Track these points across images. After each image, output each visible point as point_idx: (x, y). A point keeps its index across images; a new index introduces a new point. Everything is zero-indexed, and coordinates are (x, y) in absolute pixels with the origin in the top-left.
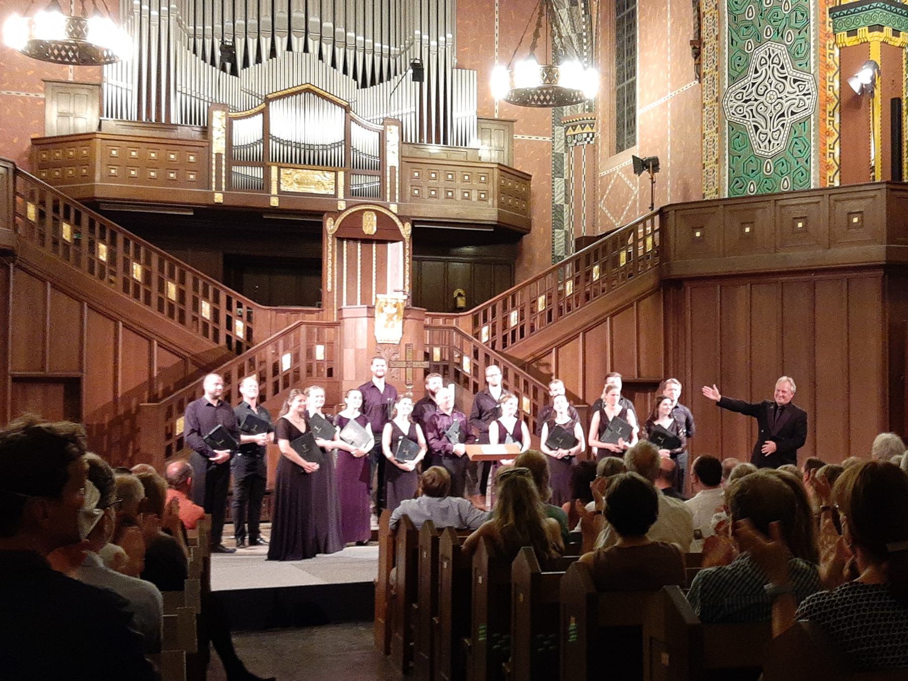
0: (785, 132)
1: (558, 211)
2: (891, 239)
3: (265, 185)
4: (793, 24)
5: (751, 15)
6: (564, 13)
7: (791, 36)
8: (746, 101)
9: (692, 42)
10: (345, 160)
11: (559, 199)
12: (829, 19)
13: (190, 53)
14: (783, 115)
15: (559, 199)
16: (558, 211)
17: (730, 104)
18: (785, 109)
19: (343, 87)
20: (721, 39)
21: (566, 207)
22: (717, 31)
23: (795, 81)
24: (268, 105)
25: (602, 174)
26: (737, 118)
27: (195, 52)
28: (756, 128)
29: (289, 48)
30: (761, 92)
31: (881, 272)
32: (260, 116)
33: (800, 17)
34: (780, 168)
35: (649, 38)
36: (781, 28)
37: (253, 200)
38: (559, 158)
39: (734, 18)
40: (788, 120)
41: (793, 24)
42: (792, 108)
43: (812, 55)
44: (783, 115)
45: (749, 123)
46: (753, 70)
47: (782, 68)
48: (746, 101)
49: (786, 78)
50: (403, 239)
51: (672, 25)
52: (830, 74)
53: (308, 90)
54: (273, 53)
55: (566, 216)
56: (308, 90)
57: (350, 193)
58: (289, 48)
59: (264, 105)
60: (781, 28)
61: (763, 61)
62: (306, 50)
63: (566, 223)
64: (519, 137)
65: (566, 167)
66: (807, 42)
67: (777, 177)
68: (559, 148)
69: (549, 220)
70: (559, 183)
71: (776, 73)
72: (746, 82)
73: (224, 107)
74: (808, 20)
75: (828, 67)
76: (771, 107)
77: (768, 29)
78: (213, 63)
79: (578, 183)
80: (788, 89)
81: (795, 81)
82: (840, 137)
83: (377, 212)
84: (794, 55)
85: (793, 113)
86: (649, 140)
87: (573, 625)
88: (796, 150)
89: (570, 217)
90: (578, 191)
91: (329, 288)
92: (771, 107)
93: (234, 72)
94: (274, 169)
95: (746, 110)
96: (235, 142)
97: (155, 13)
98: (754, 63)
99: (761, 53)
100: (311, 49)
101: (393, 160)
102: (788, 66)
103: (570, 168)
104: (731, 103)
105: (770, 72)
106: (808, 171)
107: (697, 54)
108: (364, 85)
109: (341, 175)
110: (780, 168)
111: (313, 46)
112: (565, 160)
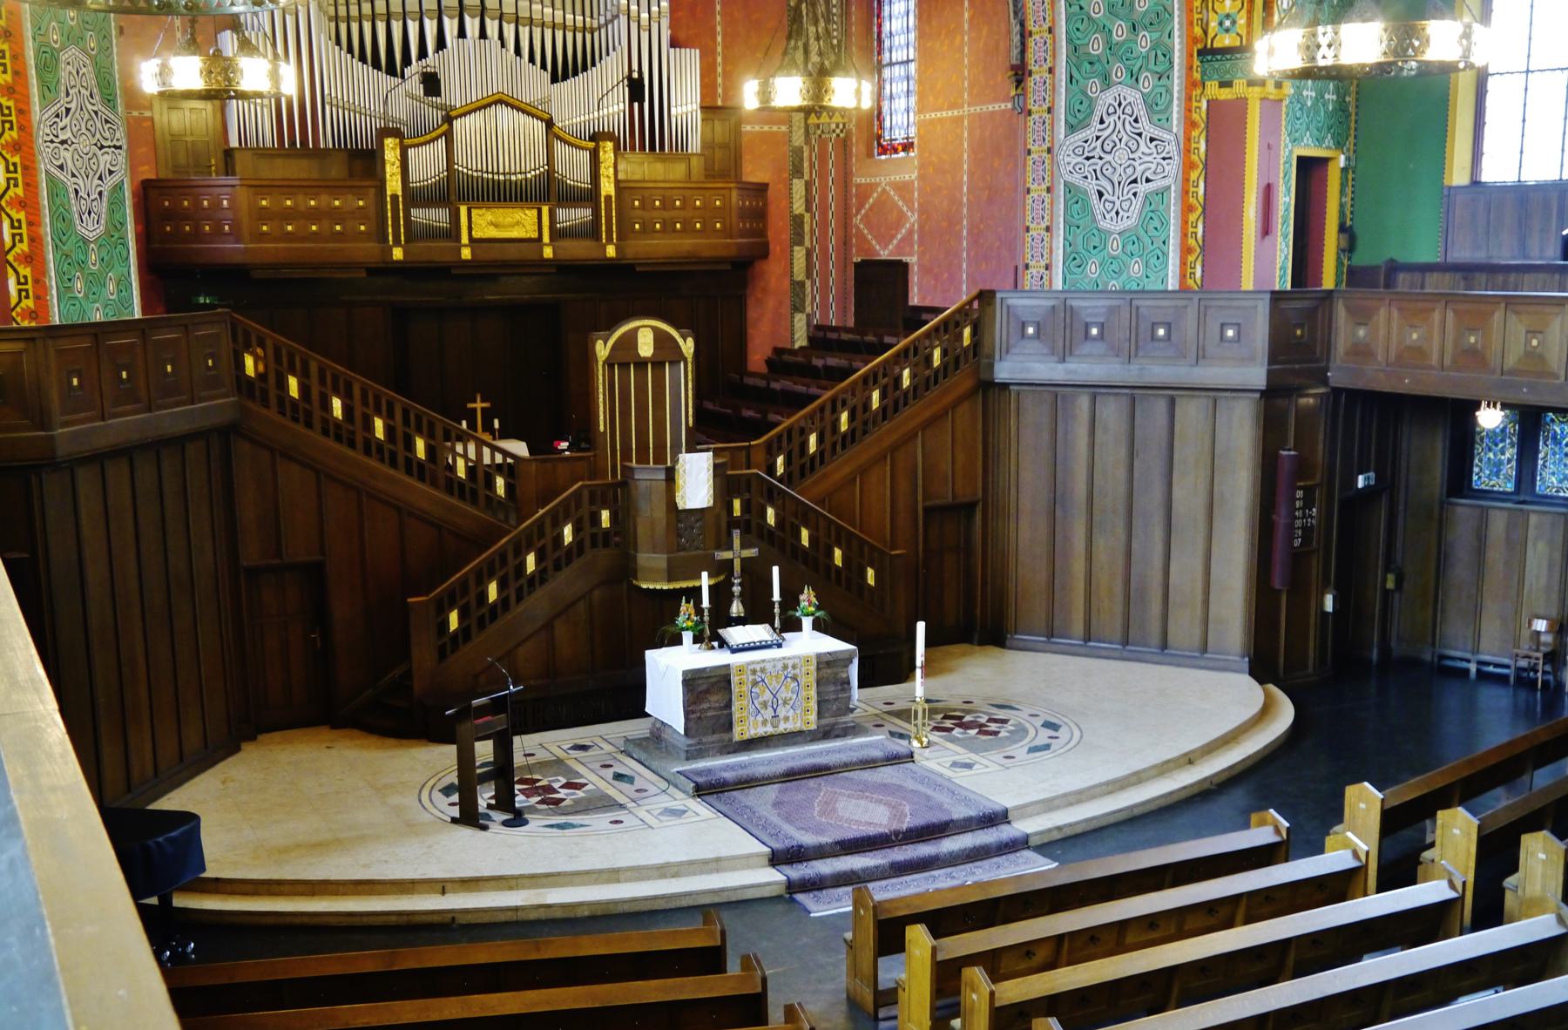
0: (1137, 204)
1: (798, 221)
2: (1273, 359)
3: (453, 233)
4: (1152, 65)
5: (1096, 48)
7: (1148, 83)
8: (1088, 158)
9: (1013, 68)
10: (545, 190)
11: (799, 207)
12: (1196, 62)
13: (331, 44)
14: (1135, 181)
16: (798, 221)
17: (1067, 159)
18: (1138, 174)
19: (534, 84)
20: (1057, 30)
21: (807, 217)
22: (1052, 58)
23: (1152, 140)
24: (451, 125)
25: (857, 180)
26: (1076, 179)
27: (338, 43)
28: (1101, 194)
29: (462, 33)
30: (1108, 148)
31: (1258, 395)
32: (442, 143)
33: (1161, 57)
34: (1130, 247)
35: (934, 23)
36: (1135, 70)
37: (435, 251)
38: (798, 152)
39: (1074, 49)
40: (1142, 188)
41: (1152, 65)
42: (1148, 174)
43: (1175, 109)
44: (1135, 181)
45: (1091, 186)
46: (1097, 119)
47: (1136, 121)
48: (1088, 158)
49: (1140, 135)
50: (685, 360)
51: (971, 19)
52: (1195, 133)
53: (500, 102)
55: (807, 228)
57: (557, 235)
58: (462, 33)
59: (445, 127)
60: (1135, 70)
61: (1111, 110)
62: (483, 35)
63: (807, 238)
64: (748, 128)
65: (806, 164)
66: (1169, 91)
67: (1125, 258)
68: (798, 139)
69: (786, 236)
70: (798, 186)
71: (1128, 127)
72: (1089, 133)
73: (396, 133)
74: (1171, 63)
75: (1193, 125)
76: (1120, 170)
77: (1118, 71)
78: (350, 50)
79: (824, 189)
80: (1143, 148)
81: (1152, 140)
82: (1204, 212)
83: (653, 328)
84: (1151, 106)
85: (1148, 180)
86: (934, 159)
87: (1375, 655)
88: (1151, 227)
89: (812, 232)
90: (824, 198)
91: (602, 428)
92: (1120, 170)
93: (391, 70)
94: (463, 210)
95: (1088, 168)
96: (413, 176)
97: (645, 16)
98: (1100, 110)
99: (1109, 98)
100: (489, 32)
102: (1144, 120)
103: (812, 166)
104: (1068, 158)
105: (1119, 125)
106: (1166, 254)
108: (554, 80)
109: (545, 210)
110: (1130, 247)
111: (492, 27)
112: (806, 154)
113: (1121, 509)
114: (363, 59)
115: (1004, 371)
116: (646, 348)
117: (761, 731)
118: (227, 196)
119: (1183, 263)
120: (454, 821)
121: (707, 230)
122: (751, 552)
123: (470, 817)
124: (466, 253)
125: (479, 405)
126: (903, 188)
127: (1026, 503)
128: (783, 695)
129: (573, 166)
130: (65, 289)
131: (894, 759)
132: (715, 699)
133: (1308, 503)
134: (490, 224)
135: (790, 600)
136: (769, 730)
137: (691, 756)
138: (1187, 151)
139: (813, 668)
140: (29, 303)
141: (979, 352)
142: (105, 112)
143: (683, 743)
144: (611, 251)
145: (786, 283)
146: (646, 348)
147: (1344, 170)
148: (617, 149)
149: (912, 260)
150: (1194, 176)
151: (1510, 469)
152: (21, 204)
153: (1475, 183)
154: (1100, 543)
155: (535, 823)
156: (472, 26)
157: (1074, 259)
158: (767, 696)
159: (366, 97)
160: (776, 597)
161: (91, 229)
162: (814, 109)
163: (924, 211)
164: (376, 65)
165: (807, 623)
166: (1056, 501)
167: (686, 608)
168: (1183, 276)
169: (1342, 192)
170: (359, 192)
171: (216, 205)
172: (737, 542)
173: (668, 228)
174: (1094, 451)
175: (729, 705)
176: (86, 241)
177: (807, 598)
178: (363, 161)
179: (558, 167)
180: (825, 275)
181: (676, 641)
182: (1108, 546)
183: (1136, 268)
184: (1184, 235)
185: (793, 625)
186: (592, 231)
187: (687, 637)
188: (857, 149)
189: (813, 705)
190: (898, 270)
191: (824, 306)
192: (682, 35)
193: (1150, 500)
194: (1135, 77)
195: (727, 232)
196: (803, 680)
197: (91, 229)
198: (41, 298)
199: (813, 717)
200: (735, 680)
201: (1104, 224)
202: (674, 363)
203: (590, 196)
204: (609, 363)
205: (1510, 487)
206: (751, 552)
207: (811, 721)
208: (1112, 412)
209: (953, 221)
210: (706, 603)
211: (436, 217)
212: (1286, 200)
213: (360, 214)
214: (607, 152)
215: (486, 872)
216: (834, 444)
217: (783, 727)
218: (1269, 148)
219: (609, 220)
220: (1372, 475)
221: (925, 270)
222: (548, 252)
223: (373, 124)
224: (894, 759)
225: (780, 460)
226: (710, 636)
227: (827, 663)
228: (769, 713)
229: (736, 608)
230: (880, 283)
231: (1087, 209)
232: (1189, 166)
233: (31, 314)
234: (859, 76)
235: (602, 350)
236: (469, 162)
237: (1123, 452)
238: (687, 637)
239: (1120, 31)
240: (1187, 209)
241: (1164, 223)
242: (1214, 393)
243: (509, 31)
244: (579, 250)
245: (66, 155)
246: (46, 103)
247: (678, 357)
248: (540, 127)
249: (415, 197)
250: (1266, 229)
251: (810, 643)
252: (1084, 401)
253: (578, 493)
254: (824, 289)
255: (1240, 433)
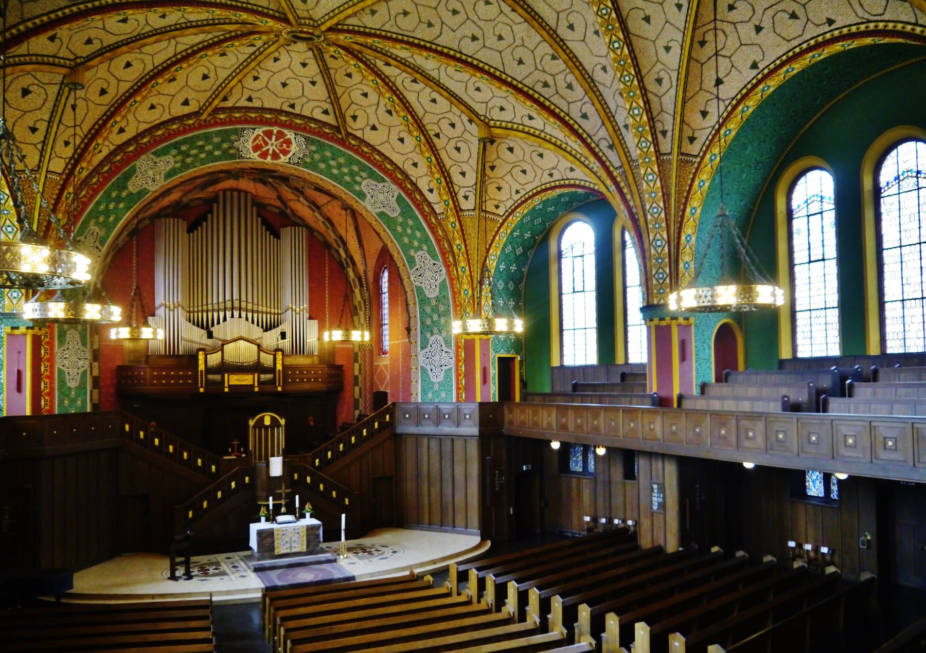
0: (443, 373)
1: (356, 378)
6: (357, 291)
10: (257, 368)
15: (357, 372)
16: (356, 378)
22: (417, 326)
25: (376, 364)
26: (424, 365)
29: (232, 316)
32: (220, 353)
38: (356, 354)
39: (422, 323)
40: (444, 368)
45: (429, 367)
54: (225, 319)
56: (441, 34)
58: (232, 316)
62: (240, 316)
70: (356, 366)
73: (203, 350)
77: (435, 330)
79: (365, 366)
87: (539, 531)
94: (226, 375)
95: (427, 362)
98: (430, 343)
99: (432, 339)
101: (279, 367)
104: (421, 358)
107: (409, 333)
108: (266, 330)
109: (256, 375)
111: (243, 314)
113: (438, 478)
114: (194, 324)
115: (400, 430)
116: (267, 421)
117: (285, 551)
118: (146, 372)
119: (458, 393)
120: (169, 578)
121: (316, 380)
122: (289, 490)
123: (173, 577)
124: (226, 390)
125: (236, 443)
126: (386, 366)
127: (409, 476)
128: (294, 538)
129: (267, 360)
130: (61, 402)
131: (328, 561)
132: (269, 540)
133: (501, 475)
134: (235, 380)
135: (302, 507)
136: (288, 551)
137: (259, 560)
138: (457, 356)
139: (305, 530)
140: (47, 408)
141: (392, 424)
142: (82, 348)
143: (257, 555)
144: (280, 389)
145: (352, 400)
146: (267, 421)
147: (521, 361)
148: (283, 354)
149: (388, 391)
150: (460, 364)
151: (580, 464)
152: (48, 377)
153: (562, 366)
154: (432, 489)
155: (195, 579)
156: (236, 313)
157: (424, 392)
158: (288, 539)
159: (193, 336)
160: (297, 505)
161: (72, 384)
162: (347, 341)
163: (391, 374)
164: (198, 326)
165: (308, 515)
166: (418, 476)
167: (263, 509)
168: (458, 397)
169: (520, 368)
170: (189, 369)
171: (139, 374)
172: (283, 487)
173: (309, 380)
174: (429, 457)
175: (273, 542)
176: (70, 389)
177: (308, 507)
178: (192, 358)
179: (262, 360)
180: (365, 396)
181: (259, 521)
182: (435, 491)
183: (443, 395)
184: (458, 384)
185: (303, 516)
186: (273, 382)
187: (263, 519)
188: (375, 352)
189: (305, 543)
190: (385, 394)
191: (365, 407)
192: (314, 315)
193: (447, 475)
194: (440, 332)
195: (323, 382)
196: (301, 534)
197: (72, 384)
198: (52, 406)
199: (305, 547)
200: (276, 533)
201: (433, 380)
202: (278, 428)
203: (272, 370)
204: (254, 427)
205: (581, 470)
206: (289, 490)
207: (304, 548)
208: (434, 444)
209: (397, 377)
210: (271, 507)
211: (217, 377)
212: (494, 372)
213: (190, 377)
214: (279, 355)
215: (169, 592)
216: (349, 447)
217: (294, 550)
218: (485, 355)
219: (279, 378)
220: (530, 466)
221: (392, 395)
222: (256, 389)
223: (196, 346)
224: (328, 561)
225: (317, 461)
226: (271, 518)
227: (311, 529)
228: (288, 545)
229: (283, 510)
230: (380, 398)
231: (428, 375)
232: (458, 361)
233: (48, 411)
234: (363, 330)
235: (251, 423)
236: (228, 358)
237: (438, 457)
238: (263, 519)
239: (435, 317)
240: (458, 375)
241: (451, 380)
242: (465, 438)
243: (250, 315)
244: (268, 388)
245: (66, 362)
246: (60, 346)
247: (279, 425)
248: (255, 348)
249: (209, 370)
250: (485, 380)
251: (309, 521)
252: (426, 441)
253: (237, 471)
254: (365, 402)
255: (473, 451)
